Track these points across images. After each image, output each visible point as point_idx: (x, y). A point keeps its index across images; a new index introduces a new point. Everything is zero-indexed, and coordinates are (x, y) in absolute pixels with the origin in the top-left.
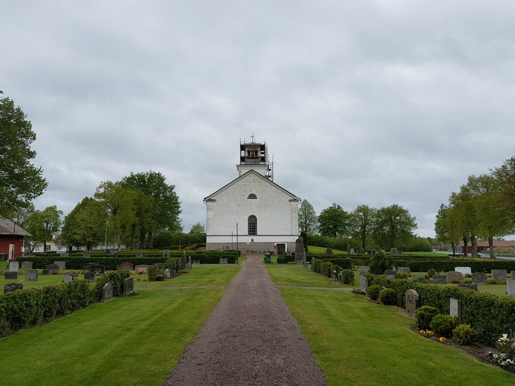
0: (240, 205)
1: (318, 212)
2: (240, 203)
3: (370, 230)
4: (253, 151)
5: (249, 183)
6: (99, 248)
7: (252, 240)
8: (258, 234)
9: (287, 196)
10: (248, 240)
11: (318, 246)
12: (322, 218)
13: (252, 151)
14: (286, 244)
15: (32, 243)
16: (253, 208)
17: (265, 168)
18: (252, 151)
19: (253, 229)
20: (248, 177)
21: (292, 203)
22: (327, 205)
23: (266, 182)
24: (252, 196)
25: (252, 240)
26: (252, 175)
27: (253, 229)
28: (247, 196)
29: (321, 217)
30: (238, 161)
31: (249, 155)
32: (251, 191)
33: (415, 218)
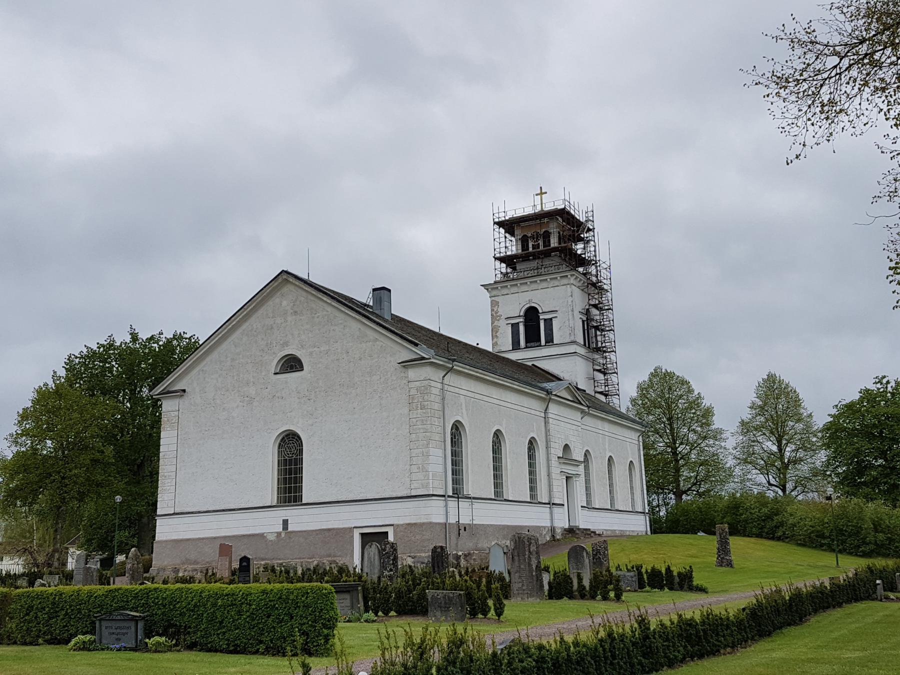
0: (252, 399)
1: (820, 409)
2: (252, 391)
4: (536, 237)
5: (279, 320)
7: (285, 523)
9: (397, 348)
10: (268, 524)
11: (759, 536)
12: (834, 432)
13: (533, 237)
14: (390, 531)
15: (19, 503)
18: (533, 237)
19: (290, 488)
20: (276, 300)
21: (412, 373)
23: (329, 309)
24: (292, 364)
25: (285, 523)
26: (287, 289)
27: (290, 488)
28: (273, 364)
29: (827, 428)
30: (494, 271)
31: (525, 247)
32: (286, 344)
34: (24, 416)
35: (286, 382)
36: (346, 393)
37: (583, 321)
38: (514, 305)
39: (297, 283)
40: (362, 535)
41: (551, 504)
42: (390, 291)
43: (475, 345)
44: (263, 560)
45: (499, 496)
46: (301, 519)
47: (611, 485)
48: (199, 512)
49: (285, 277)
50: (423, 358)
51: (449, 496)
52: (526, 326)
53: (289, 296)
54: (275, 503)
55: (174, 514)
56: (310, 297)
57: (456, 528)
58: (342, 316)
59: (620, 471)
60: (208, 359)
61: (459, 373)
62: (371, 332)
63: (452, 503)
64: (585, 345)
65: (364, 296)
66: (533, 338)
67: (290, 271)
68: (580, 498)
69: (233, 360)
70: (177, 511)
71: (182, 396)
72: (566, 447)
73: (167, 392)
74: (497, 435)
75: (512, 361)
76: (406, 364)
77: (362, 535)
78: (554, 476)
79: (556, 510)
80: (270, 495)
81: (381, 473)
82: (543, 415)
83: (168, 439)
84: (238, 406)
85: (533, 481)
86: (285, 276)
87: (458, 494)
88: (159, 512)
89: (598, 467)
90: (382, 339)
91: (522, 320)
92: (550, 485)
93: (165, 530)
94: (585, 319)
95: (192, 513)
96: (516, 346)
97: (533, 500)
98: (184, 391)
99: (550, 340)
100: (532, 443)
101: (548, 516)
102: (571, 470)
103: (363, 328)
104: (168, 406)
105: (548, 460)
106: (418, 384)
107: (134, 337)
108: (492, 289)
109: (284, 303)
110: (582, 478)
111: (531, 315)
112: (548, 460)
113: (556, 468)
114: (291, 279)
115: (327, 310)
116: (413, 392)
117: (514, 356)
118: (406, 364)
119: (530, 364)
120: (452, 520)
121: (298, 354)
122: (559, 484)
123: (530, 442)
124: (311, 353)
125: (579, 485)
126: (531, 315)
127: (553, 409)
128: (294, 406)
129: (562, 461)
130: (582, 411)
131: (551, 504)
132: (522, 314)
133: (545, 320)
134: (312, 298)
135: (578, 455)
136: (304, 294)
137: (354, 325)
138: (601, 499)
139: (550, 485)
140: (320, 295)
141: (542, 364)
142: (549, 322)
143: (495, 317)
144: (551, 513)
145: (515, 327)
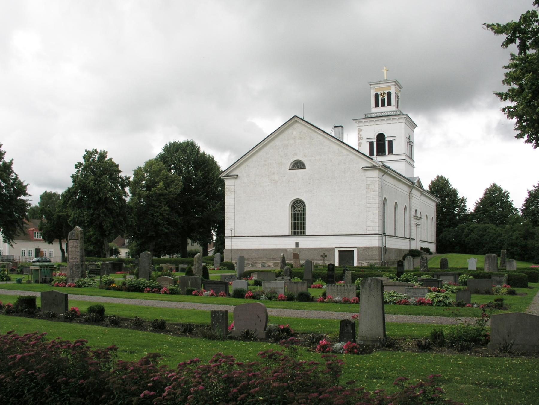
3: (90, 182)
6: (173, 230)
7: (297, 244)
8: (307, 234)
9: (359, 160)
10: (289, 243)
16: (298, 186)
17: (401, 121)
19: (298, 224)
20: (290, 131)
22: (433, 178)
23: (321, 138)
24: (298, 165)
25: (297, 244)
26: (296, 125)
27: (298, 224)
28: (288, 165)
32: (296, 154)
33: (534, 186)
38: (371, 131)
40: (339, 251)
46: (305, 243)
50: (376, 167)
52: (377, 144)
53: (298, 129)
59: (429, 221)
60: (251, 160)
66: (381, 151)
70: (236, 235)
71: (236, 178)
77: (339, 251)
79: (412, 241)
83: (229, 200)
86: (296, 119)
88: (226, 235)
92: (410, 229)
95: (395, 228)
98: (238, 175)
99: (391, 151)
101: (409, 244)
102: (418, 222)
106: (372, 179)
107: (535, 187)
109: (295, 133)
111: (381, 137)
113: (413, 221)
114: (299, 121)
116: (369, 183)
118: (365, 168)
124: (310, 160)
126: (381, 137)
127: (414, 191)
130: (421, 192)
131: (410, 239)
132: (375, 137)
134: (311, 131)
136: (306, 129)
139: (410, 229)
140: (316, 130)
142: (390, 143)
145: (371, 144)
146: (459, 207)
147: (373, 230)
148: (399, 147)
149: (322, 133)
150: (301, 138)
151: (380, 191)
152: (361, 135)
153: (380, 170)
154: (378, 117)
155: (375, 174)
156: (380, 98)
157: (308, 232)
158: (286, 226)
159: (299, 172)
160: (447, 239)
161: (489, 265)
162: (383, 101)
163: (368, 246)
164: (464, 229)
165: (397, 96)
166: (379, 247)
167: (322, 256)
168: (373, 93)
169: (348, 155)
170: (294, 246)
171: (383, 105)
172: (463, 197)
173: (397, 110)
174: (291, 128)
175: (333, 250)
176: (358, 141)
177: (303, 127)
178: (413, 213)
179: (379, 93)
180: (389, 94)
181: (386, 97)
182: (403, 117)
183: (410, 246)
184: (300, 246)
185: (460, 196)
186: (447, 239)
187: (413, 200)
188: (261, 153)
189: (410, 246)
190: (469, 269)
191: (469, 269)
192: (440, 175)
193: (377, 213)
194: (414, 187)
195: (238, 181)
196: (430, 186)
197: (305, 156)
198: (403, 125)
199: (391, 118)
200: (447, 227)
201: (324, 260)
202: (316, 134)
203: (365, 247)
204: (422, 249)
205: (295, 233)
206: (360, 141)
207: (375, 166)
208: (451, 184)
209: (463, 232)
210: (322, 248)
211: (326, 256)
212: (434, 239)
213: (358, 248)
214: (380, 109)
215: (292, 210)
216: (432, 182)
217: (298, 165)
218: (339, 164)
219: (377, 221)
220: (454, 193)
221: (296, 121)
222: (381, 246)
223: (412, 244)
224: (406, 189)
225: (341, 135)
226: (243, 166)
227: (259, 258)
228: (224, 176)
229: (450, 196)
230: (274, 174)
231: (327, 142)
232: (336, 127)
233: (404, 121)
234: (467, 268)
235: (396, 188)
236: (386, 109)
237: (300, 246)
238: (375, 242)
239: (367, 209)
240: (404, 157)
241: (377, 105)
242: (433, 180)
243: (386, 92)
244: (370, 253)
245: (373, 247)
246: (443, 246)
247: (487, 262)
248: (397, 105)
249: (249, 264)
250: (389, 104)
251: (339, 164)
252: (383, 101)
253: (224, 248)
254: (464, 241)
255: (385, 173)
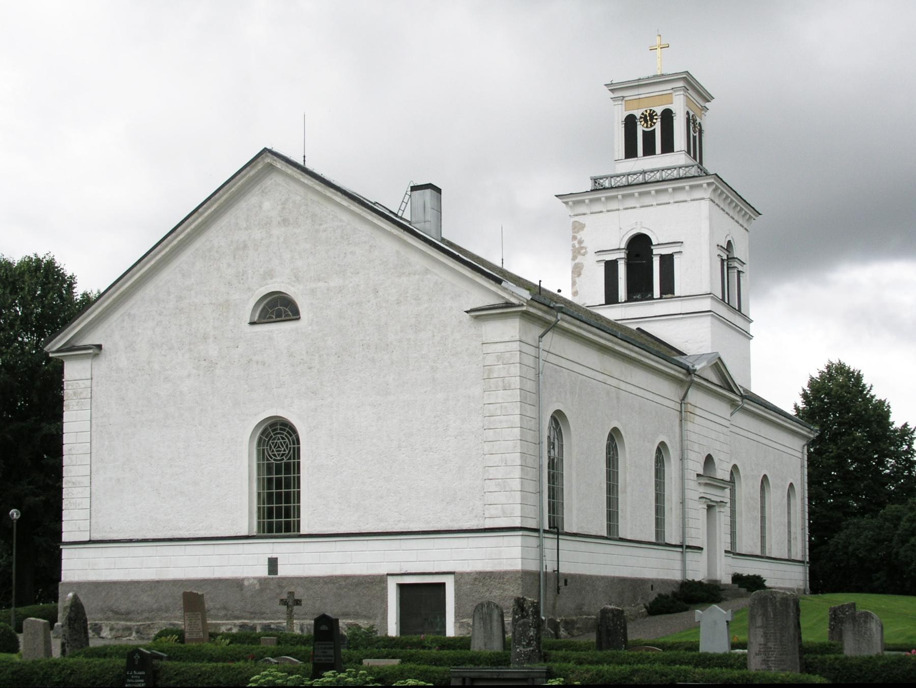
2: (213, 351)
5: (258, 234)
7: (273, 564)
8: (304, 530)
9: (462, 286)
10: (248, 562)
17: (698, 194)
19: (278, 509)
20: (252, 199)
23: (345, 217)
24: (278, 308)
25: (273, 564)
26: (273, 182)
27: (278, 509)
28: (247, 307)
32: (269, 274)
34: (888, 412)
35: (270, 338)
36: (373, 360)
37: (723, 261)
38: (610, 231)
39: (290, 170)
40: (402, 587)
41: (684, 547)
42: (439, 191)
43: (556, 292)
44: (237, 618)
45: (612, 535)
46: (299, 560)
47: (763, 518)
48: (131, 541)
49: (266, 163)
50: (511, 305)
51: (545, 531)
53: (273, 197)
54: (254, 532)
55: (91, 542)
56: (311, 196)
57: (552, 584)
58: (366, 230)
59: (776, 496)
61: (566, 332)
62: (418, 259)
63: (549, 543)
64: (723, 299)
65: (393, 199)
66: (640, 289)
67: (275, 150)
68: (723, 541)
69: (180, 298)
70: (96, 536)
71: (96, 355)
72: (709, 460)
73: (70, 348)
74: (614, 437)
75: (608, 321)
76: (479, 314)
77: (402, 587)
78: (690, 504)
79: (691, 556)
80: (244, 519)
81: (427, 488)
82: (678, 407)
84: (189, 376)
85: (660, 510)
86: (269, 159)
87: (556, 528)
88: (65, 537)
89: (747, 489)
90: (437, 270)
91: (623, 255)
93: (76, 567)
94: (725, 257)
96: (611, 298)
97: (660, 542)
98: (99, 347)
99: (668, 288)
100: (662, 449)
102: (715, 495)
103: (403, 251)
104: (75, 373)
105: (683, 478)
106: (500, 348)
108: (575, 203)
109: (267, 205)
110: (727, 510)
111: (639, 246)
112: (683, 478)
113: (695, 491)
114: (279, 164)
115: (339, 218)
116: (490, 360)
117: (612, 313)
118: (479, 314)
119: (634, 327)
120: (550, 567)
121: (292, 291)
122: (698, 513)
123: (659, 451)
124: (313, 292)
125: (723, 517)
126: (639, 246)
127: (695, 396)
128: (278, 377)
129: (703, 481)
130: (733, 403)
131: (684, 547)
132: (623, 246)
133: (662, 257)
134: (315, 198)
135: (722, 472)
136: (301, 190)
137: (388, 246)
138: (636, 520)
140: (329, 192)
141: (652, 328)
142: (667, 261)
143: (578, 251)
144: (684, 561)
145: (611, 267)
146: (896, 455)
147: (505, 515)
148: (695, 273)
149: (345, 202)
150: (285, 222)
151: (530, 386)
152: (580, 242)
153: (525, 315)
154: (629, 185)
155: (509, 330)
156: (640, 129)
157: (308, 522)
158: (239, 506)
159: (280, 330)
160: (851, 548)
161: (765, 635)
162: (649, 137)
163: (489, 569)
164: (899, 518)
165: (690, 121)
166: (525, 574)
167: (284, 602)
168: (620, 114)
169: (427, 271)
170: (262, 571)
171: (649, 150)
172: (906, 425)
173: (690, 161)
174: (256, 190)
175: (380, 581)
176: (574, 258)
177: (294, 187)
178: (696, 466)
179: (638, 113)
180: (667, 117)
181: (658, 127)
182: (704, 182)
183: (684, 570)
184: (283, 571)
185: (897, 420)
186: (851, 548)
187: (695, 427)
188: (167, 275)
189: (684, 570)
190: (703, 649)
191: (703, 649)
192: (835, 361)
193: (516, 459)
194: (692, 383)
195: (101, 366)
196: (805, 395)
197: (298, 279)
198: (705, 205)
199: (670, 186)
200: (855, 515)
201: (290, 617)
202: (330, 208)
203: (480, 573)
204: (737, 578)
205: (270, 530)
206: (580, 259)
207: (508, 305)
208: (868, 387)
209: (896, 526)
210: (346, 578)
211: (298, 602)
212: (800, 549)
213: (459, 576)
214: (642, 163)
215: (261, 455)
216: (812, 383)
217: (278, 308)
218: (399, 303)
219: (516, 484)
220: (881, 412)
221: (271, 168)
222: (533, 567)
223: (690, 565)
224: (667, 391)
225: (430, 215)
226: (115, 318)
227: (159, 610)
228: (58, 351)
229: (868, 423)
230: (205, 338)
231: (364, 231)
232: (414, 188)
233: (707, 193)
234: (695, 647)
235: (610, 381)
236: (660, 160)
237: (283, 571)
238: (509, 555)
239: (487, 447)
240: (706, 304)
241: (630, 152)
242: (816, 375)
243: (659, 110)
244: (496, 593)
245: (506, 573)
246: (831, 566)
247: (759, 622)
248: (695, 148)
249: (129, 629)
250: (668, 147)
251: (399, 303)
252: (649, 137)
253: (60, 579)
254: (897, 554)
255: (550, 327)
